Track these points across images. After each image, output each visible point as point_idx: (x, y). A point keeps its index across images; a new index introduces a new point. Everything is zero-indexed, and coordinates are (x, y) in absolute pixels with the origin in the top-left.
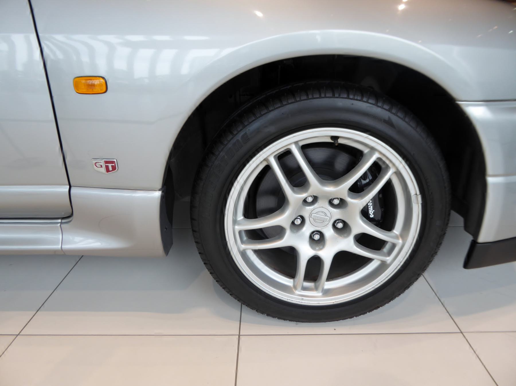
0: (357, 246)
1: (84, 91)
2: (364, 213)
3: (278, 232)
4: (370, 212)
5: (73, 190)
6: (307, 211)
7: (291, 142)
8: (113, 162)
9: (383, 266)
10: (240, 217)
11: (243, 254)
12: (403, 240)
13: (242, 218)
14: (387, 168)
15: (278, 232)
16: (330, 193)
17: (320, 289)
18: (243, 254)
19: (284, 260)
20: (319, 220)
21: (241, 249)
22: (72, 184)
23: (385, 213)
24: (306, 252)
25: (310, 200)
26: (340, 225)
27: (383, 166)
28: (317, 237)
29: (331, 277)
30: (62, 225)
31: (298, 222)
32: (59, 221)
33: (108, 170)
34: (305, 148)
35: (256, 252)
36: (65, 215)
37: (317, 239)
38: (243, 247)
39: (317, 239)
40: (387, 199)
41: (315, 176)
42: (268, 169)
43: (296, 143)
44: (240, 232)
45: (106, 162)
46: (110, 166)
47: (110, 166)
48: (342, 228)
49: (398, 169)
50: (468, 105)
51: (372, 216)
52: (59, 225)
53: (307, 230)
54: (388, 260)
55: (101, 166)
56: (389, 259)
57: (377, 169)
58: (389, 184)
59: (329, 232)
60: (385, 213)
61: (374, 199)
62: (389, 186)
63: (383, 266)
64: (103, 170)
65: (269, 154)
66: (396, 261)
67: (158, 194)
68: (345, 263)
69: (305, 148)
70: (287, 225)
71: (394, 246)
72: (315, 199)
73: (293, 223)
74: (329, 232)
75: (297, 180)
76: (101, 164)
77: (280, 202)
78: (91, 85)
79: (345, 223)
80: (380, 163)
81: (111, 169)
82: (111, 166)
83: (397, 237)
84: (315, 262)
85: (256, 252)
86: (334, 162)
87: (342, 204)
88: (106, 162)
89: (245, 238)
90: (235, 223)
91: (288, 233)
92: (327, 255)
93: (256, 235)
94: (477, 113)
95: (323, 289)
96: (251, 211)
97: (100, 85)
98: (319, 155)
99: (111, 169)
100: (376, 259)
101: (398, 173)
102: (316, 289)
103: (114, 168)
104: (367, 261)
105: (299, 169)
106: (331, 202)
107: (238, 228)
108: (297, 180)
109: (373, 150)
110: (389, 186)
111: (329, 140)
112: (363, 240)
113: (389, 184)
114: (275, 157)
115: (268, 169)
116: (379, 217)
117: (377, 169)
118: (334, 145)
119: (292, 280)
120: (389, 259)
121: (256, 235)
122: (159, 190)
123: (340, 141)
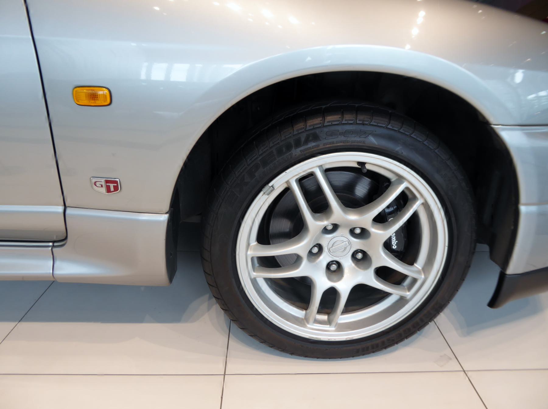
0: (377, 280)
1: (86, 102)
2: (387, 245)
3: (295, 260)
4: (393, 243)
5: (68, 211)
6: (326, 240)
7: (314, 165)
8: (116, 182)
9: (402, 302)
10: (254, 243)
11: (254, 282)
12: (425, 274)
13: (256, 243)
14: (415, 198)
15: (295, 260)
16: (352, 221)
17: (334, 324)
18: (254, 282)
19: (297, 291)
20: (337, 250)
21: (252, 277)
22: (67, 205)
23: (408, 246)
24: (322, 283)
25: (330, 227)
26: (360, 256)
27: (410, 196)
28: (334, 267)
29: (348, 309)
30: (54, 249)
31: (315, 250)
32: (51, 244)
33: (109, 190)
34: (327, 171)
35: (267, 280)
36: (59, 240)
37: (335, 269)
38: (254, 274)
39: (335, 269)
40: (411, 233)
41: (332, 194)
42: (287, 190)
43: (320, 167)
44: (252, 259)
45: (107, 182)
46: (112, 186)
47: (112, 186)
48: (361, 258)
49: (426, 201)
50: (504, 130)
51: (394, 247)
52: (50, 248)
53: (324, 259)
54: (408, 295)
55: (102, 186)
56: (408, 294)
57: (404, 200)
58: (415, 216)
59: (347, 263)
60: (408, 246)
61: (397, 233)
62: (414, 219)
63: (402, 302)
64: (104, 190)
65: (289, 177)
66: (416, 298)
67: (164, 218)
68: (362, 296)
69: (327, 171)
70: (304, 254)
71: (415, 281)
72: (335, 227)
73: (310, 252)
74: (347, 263)
75: (320, 206)
76: (101, 183)
77: (298, 228)
78: (93, 96)
79: (364, 253)
80: (407, 192)
81: (112, 189)
82: (112, 186)
83: (419, 272)
84: (331, 295)
85: (267, 280)
86: (361, 189)
87: (364, 234)
88: (107, 182)
89: (257, 264)
90: (247, 247)
91: (305, 262)
92: (344, 287)
93: (269, 263)
94: (511, 138)
95: (337, 323)
96: (264, 237)
97: (105, 96)
98: (342, 178)
99: (112, 189)
100: (395, 293)
101: (426, 205)
102: (329, 322)
103: (116, 188)
104: (385, 295)
105: (319, 189)
106: (352, 232)
107: (250, 253)
108: (320, 206)
109: (401, 179)
110: (414, 219)
111: (356, 165)
112: (383, 273)
113: (415, 216)
114: (296, 180)
115: (287, 190)
116: (402, 248)
117: (404, 200)
118: (360, 170)
119: (304, 312)
120: (408, 294)
121: (269, 263)
122: (166, 213)
123: (368, 167)
